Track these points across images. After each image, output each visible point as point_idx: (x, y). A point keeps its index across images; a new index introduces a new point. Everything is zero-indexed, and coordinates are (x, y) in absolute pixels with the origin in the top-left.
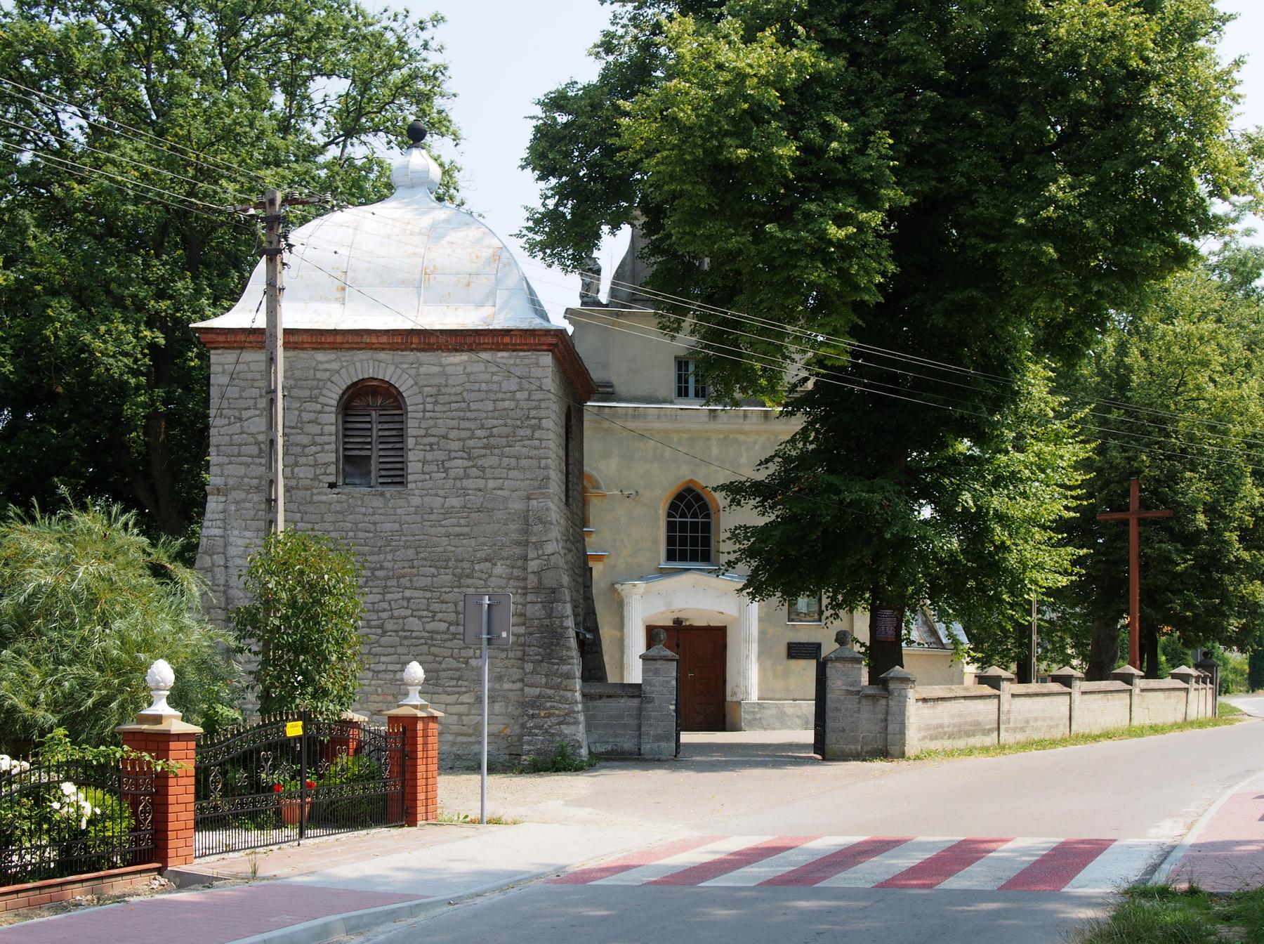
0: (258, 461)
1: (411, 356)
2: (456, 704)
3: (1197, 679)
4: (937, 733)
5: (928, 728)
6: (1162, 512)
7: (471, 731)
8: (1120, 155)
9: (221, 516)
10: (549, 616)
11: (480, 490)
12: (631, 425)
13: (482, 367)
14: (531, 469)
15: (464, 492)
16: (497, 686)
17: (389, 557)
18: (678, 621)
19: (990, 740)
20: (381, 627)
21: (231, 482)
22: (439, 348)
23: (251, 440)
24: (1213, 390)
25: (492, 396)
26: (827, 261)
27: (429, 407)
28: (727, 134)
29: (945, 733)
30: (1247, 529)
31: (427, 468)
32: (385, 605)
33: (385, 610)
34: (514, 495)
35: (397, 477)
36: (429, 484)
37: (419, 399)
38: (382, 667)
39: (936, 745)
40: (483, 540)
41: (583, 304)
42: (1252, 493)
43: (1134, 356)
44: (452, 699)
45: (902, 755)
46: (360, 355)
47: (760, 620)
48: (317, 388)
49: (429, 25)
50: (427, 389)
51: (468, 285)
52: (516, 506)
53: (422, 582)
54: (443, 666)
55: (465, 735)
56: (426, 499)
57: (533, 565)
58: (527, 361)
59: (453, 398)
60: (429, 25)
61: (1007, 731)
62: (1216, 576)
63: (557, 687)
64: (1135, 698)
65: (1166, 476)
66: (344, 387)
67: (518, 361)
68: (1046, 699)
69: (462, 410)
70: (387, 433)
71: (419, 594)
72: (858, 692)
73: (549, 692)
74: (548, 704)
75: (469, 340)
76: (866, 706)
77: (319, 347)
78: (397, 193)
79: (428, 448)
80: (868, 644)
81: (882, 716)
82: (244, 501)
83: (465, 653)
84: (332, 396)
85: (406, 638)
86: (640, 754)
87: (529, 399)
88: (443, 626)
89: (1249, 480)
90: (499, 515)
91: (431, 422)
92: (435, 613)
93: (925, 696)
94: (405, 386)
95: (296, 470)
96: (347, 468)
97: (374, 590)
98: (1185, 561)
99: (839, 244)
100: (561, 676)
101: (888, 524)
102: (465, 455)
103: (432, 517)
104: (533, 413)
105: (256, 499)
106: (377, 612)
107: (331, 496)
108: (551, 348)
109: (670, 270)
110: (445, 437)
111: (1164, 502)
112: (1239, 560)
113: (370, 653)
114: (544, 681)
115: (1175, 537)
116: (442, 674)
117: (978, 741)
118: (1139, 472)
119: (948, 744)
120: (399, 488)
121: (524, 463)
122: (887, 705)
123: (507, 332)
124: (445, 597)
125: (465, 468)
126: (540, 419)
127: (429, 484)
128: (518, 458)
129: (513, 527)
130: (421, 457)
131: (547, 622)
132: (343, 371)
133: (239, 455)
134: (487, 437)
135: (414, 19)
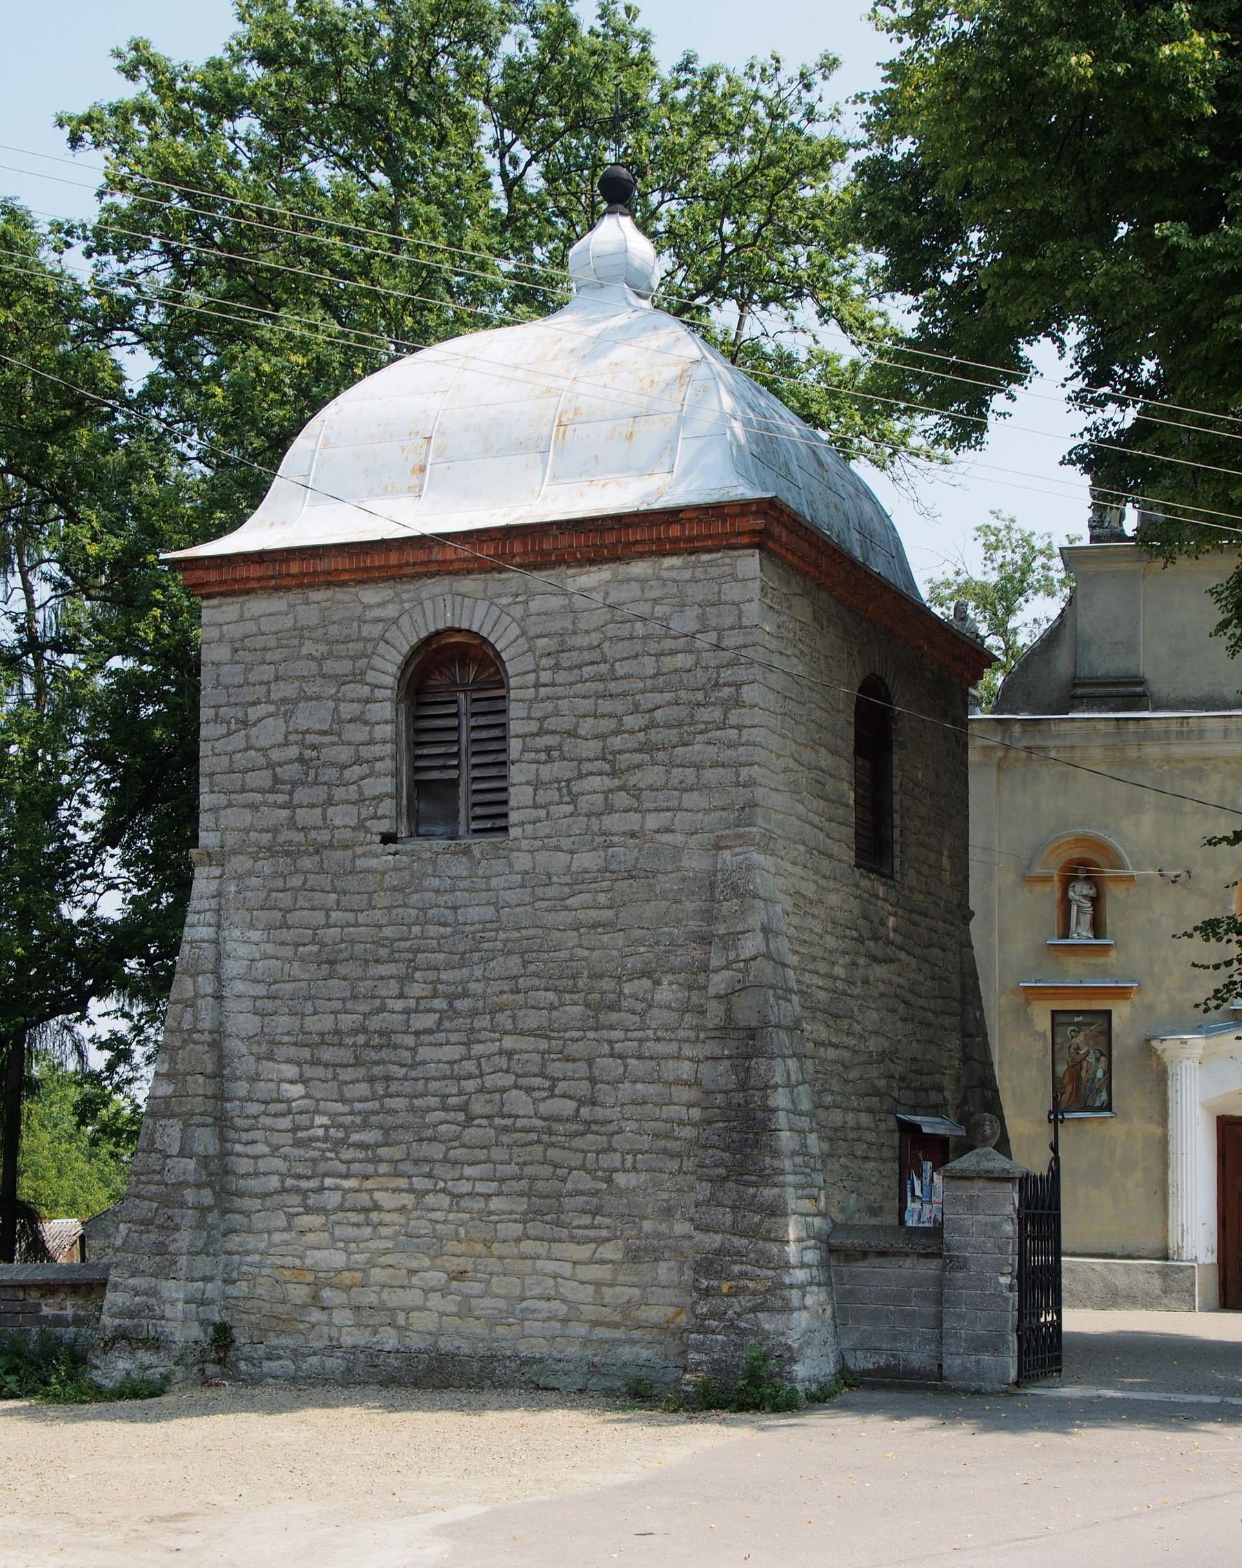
0: (271, 798)
1: (514, 579)
2: (592, 1261)
7: (617, 1318)
10: (743, 1086)
11: (633, 835)
13: (634, 591)
14: (721, 787)
15: (604, 841)
16: (663, 1227)
17: (478, 973)
20: (464, 1108)
21: (231, 840)
23: (262, 761)
25: (653, 647)
27: (545, 677)
31: (542, 797)
32: (470, 1066)
33: (470, 1077)
35: (495, 822)
36: (544, 828)
38: (465, 1187)
40: (638, 933)
41: (1093, 538)
44: (583, 1252)
46: (432, 587)
49: (817, 77)
50: (541, 642)
51: (630, 437)
52: (695, 863)
53: (531, 1020)
54: (569, 1186)
56: (542, 857)
57: (719, 982)
58: (714, 572)
59: (587, 656)
60: (817, 77)
63: (753, 1233)
66: (406, 649)
67: (699, 573)
69: (601, 679)
70: (484, 734)
71: (528, 1043)
73: (738, 1242)
74: (736, 1268)
75: (609, 538)
77: (365, 578)
79: (543, 756)
82: (250, 873)
84: (387, 668)
85: (505, 1129)
86: (941, 1377)
87: (718, 647)
88: (568, 1107)
90: (666, 883)
91: (549, 706)
92: (555, 1080)
94: (505, 640)
95: (331, 811)
96: (423, 806)
97: (454, 1037)
100: (761, 1209)
102: (607, 767)
103: (551, 892)
104: (726, 675)
107: (384, 859)
108: (760, 541)
110: (572, 734)
113: (445, 1160)
114: (728, 1219)
116: (568, 1203)
120: (497, 839)
121: (710, 775)
123: (672, 515)
124: (572, 1049)
125: (607, 793)
126: (738, 686)
127: (544, 828)
128: (698, 767)
129: (690, 906)
130: (531, 776)
131: (738, 1097)
132: (404, 621)
134: (644, 729)
135: (790, 70)
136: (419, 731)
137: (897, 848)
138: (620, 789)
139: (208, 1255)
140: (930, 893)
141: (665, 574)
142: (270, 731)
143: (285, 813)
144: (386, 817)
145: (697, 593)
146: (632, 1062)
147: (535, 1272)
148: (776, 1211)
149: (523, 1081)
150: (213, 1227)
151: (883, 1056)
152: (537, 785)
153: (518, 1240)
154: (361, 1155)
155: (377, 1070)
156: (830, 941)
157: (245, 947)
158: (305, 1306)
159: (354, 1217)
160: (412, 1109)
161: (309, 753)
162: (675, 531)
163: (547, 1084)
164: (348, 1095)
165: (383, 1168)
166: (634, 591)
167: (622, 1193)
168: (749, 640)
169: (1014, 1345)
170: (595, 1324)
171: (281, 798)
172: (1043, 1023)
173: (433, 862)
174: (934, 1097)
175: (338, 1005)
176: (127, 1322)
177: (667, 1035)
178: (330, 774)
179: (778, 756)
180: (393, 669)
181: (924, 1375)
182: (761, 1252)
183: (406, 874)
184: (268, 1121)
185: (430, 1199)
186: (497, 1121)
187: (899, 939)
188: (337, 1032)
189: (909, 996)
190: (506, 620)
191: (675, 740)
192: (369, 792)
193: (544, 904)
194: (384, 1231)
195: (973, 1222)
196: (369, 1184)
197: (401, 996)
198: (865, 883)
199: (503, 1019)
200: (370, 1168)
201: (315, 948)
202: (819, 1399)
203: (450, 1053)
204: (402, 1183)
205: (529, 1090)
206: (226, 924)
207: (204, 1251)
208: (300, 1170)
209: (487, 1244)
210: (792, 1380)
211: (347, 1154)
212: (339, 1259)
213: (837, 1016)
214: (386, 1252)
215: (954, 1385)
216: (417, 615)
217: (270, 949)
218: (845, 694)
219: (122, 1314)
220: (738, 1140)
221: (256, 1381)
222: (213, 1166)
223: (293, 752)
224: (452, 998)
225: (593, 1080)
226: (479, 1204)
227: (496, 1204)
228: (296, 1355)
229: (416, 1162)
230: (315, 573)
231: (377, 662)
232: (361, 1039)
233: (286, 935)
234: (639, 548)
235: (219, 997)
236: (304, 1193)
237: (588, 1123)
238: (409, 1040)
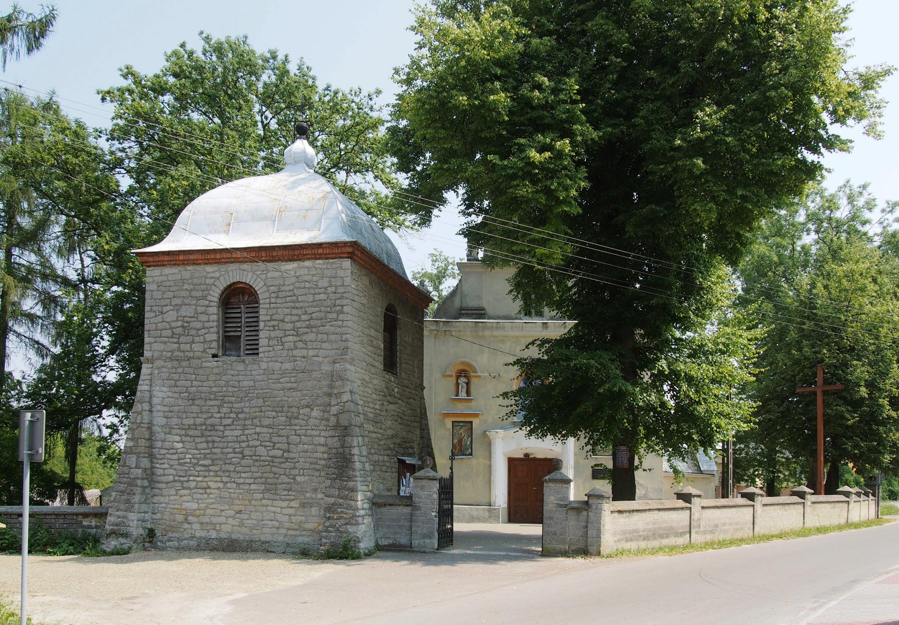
0: (171, 340)
3: (858, 494)
4: (633, 535)
5: (624, 532)
6: (838, 386)
7: (297, 527)
8: (766, 107)
9: (149, 377)
10: (343, 446)
12: (495, 333)
14: (336, 342)
15: (294, 359)
16: (314, 495)
17: (247, 405)
18: (527, 455)
19: (682, 540)
22: (279, 260)
23: (168, 326)
24: (870, 307)
25: (312, 291)
26: (534, 181)
27: (273, 300)
28: (454, 87)
29: (640, 536)
30: (894, 397)
32: (244, 438)
33: (244, 442)
34: (326, 360)
35: (254, 351)
36: (272, 354)
38: (242, 481)
39: (633, 545)
40: (305, 392)
41: (468, 260)
42: (898, 372)
43: (820, 289)
44: (285, 504)
45: (598, 554)
46: (232, 267)
47: (575, 454)
48: (207, 290)
49: (374, 96)
51: (305, 217)
52: (326, 368)
53: (266, 422)
55: (293, 529)
56: (271, 364)
57: (334, 410)
58: (334, 266)
59: (288, 294)
60: (374, 96)
61: (697, 533)
62: (874, 427)
63: (346, 498)
64: (808, 509)
65: (841, 364)
66: (222, 288)
67: (329, 266)
68: (733, 510)
70: (250, 320)
71: (265, 430)
73: (341, 501)
74: (339, 510)
75: (297, 252)
76: (572, 516)
77: (207, 262)
78: (286, 167)
81: (584, 524)
82: (163, 367)
83: (293, 472)
84: (215, 295)
85: (257, 460)
88: (280, 453)
89: (896, 366)
90: (315, 374)
91: (274, 311)
93: (620, 509)
94: (258, 286)
95: (193, 345)
97: (238, 427)
98: (854, 418)
99: (542, 166)
100: (348, 489)
101: (602, 383)
102: (295, 333)
103: (274, 377)
104: (338, 302)
105: (170, 366)
106: (240, 442)
107: (213, 363)
108: (351, 256)
111: (839, 380)
112: (889, 417)
113: (234, 471)
114: (337, 493)
115: (847, 402)
116: (279, 487)
117: (672, 541)
118: (822, 360)
119: (643, 544)
120: (255, 357)
121: (332, 337)
123: (320, 245)
124: (281, 432)
126: (343, 306)
127: (272, 354)
128: (328, 334)
129: (324, 383)
131: (341, 450)
132: (222, 278)
133: (161, 337)
135: (365, 93)
136: (227, 318)
142: (171, 316)
144: (214, 348)
145: (328, 273)
148: (354, 490)
151: (393, 436)
152: (270, 338)
153: (261, 500)
154: (203, 469)
155: (209, 439)
156: (374, 396)
157: (161, 393)
158: (182, 522)
159: (201, 491)
161: (185, 324)
162: (320, 251)
165: (211, 474)
167: (299, 483)
169: (437, 536)
171: (175, 340)
172: (450, 426)
173: (231, 365)
174: (411, 451)
175: (195, 415)
180: (217, 295)
183: (221, 369)
185: (229, 485)
186: (254, 457)
187: (398, 396)
188: (195, 425)
194: (212, 496)
195: (423, 494)
196: (206, 479)
199: (256, 421)
200: (207, 474)
202: (369, 555)
203: (239, 433)
204: (219, 479)
205: (265, 447)
207: (145, 502)
209: (250, 501)
216: (226, 276)
217: (170, 394)
218: (380, 310)
221: (163, 549)
223: (180, 323)
225: (289, 444)
227: (253, 487)
228: (179, 540)
232: (204, 427)
233: (176, 389)
236: (182, 482)
237: (287, 459)
238: (222, 428)
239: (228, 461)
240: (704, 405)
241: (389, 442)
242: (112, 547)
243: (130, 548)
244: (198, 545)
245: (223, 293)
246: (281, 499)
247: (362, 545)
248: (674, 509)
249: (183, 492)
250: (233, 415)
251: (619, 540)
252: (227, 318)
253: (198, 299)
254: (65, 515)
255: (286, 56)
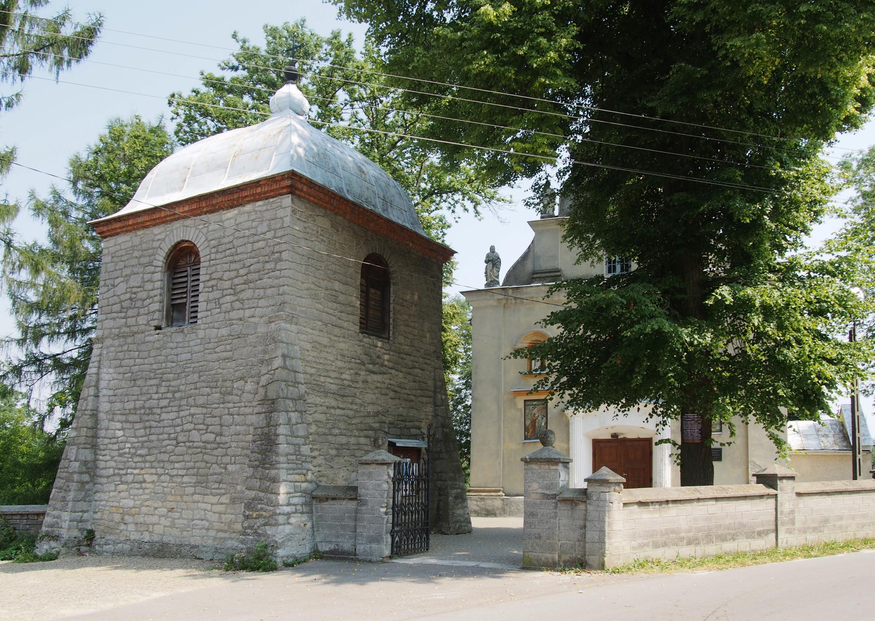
7: (226, 528)
10: (268, 425)
11: (241, 320)
17: (183, 382)
18: (615, 436)
20: (176, 439)
22: (221, 208)
26: (493, 46)
29: (682, 539)
32: (179, 421)
36: (209, 319)
37: (207, 251)
38: (175, 472)
39: (668, 553)
40: (240, 361)
44: (214, 500)
45: (602, 567)
46: (177, 224)
51: (257, 158)
52: (262, 329)
53: (201, 400)
54: (211, 471)
55: (222, 531)
56: (208, 331)
57: (264, 380)
58: (274, 206)
59: (228, 246)
61: (789, 531)
63: (266, 490)
66: (166, 250)
72: (554, 496)
73: (261, 494)
74: (259, 506)
76: (564, 511)
77: (156, 223)
80: (679, 442)
81: (580, 522)
82: (112, 346)
84: (160, 259)
85: (189, 447)
86: (355, 555)
90: (251, 339)
91: (213, 268)
97: (174, 409)
102: (232, 292)
103: (210, 346)
107: (153, 336)
108: (292, 191)
109: (581, 204)
110: (221, 279)
114: (258, 484)
119: (686, 551)
122: (586, 510)
123: (256, 183)
126: (281, 252)
127: (209, 319)
131: (266, 430)
136: (174, 284)
137: (391, 326)
138: (237, 300)
139: (85, 501)
140: (413, 346)
141: (257, 209)
142: (121, 288)
143: (124, 320)
144: (158, 318)
145: (268, 215)
146: (236, 416)
147: (198, 508)
148: (275, 480)
149: (198, 427)
150: (89, 490)
151: (377, 414)
152: (208, 301)
153: (193, 495)
154: (140, 459)
155: (147, 424)
156: (340, 364)
157: (108, 375)
158: (119, 523)
159: (137, 486)
160: (158, 440)
161: (134, 296)
162: (259, 190)
163: (205, 427)
164: (137, 434)
165: (147, 465)
166: (245, 217)
167: (230, 474)
168: (286, 232)
170: (219, 531)
171: (123, 315)
172: (521, 405)
173: (171, 336)
175: (135, 397)
176: (50, 529)
177: (249, 404)
178: (139, 303)
179: (303, 283)
180: (162, 259)
181: (349, 554)
182: (269, 499)
183: (161, 342)
184: (110, 446)
185: (162, 477)
186: (187, 444)
187: (391, 365)
188: (135, 409)
189: (396, 389)
190: (201, 234)
191: (257, 278)
192: (152, 310)
193: (207, 351)
194: (147, 491)
195: (370, 484)
196: (143, 472)
197: (157, 393)
198: (366, 340)
199: (191, 400)
200: (143, 465)
201: (130, 375)
202: (293, 564)
203: (173, 415)
204: (153, 471)
205: (199, 430)
206: (102, 367)
207: (84, 500)
208: (120, 466)
209: (182, 496)
210: (276, 557)
211: (136, 459)
212: (130, 503)
213: (344, 396)
214: (147, 500)
215: (360, 558)
216: (171, 237)
217: (115, 376)
218: (354, 261)
219: (48, 526)
220: (265, 446)
221: (100, 554)
222: (89, 465)
223: (128, 296)
224: (174, 392)
225: (221, 425)
226: (179, 480)
227: (186, 479)
228: (115, 543)
229: (159, 462)
230: (137, 224)
231: (157, 257)
232: (142, 411)
233: (121, 370)
234: (247, 199)
235: (97, 396)
236: (120, 475)
237: (219, 444)
238: (158, 411)
239: (163, 450)
240: (797, 349)
241: (370, 421)
242: (44, 551)
243: (58, 553)
244: (131, 550)
245: (168, 256)
246: (211, 494)
247: (281, 552)
248: (745, 498)
249: (122, 487)
250: (169, 395)
251: (642, 546)
252: (174, 284)
253: (145, 266)
254: (28, 515)
255: (350, 35)
